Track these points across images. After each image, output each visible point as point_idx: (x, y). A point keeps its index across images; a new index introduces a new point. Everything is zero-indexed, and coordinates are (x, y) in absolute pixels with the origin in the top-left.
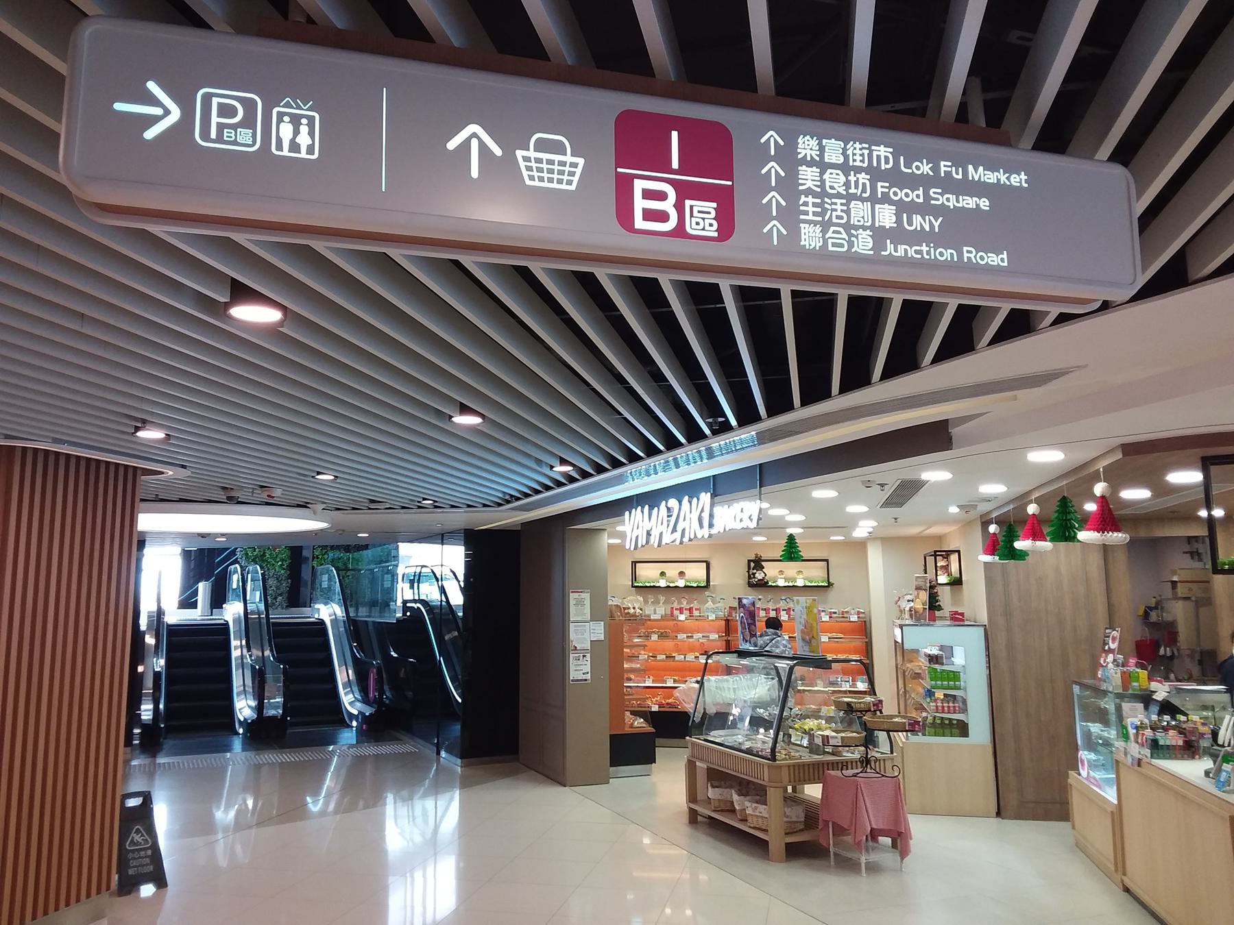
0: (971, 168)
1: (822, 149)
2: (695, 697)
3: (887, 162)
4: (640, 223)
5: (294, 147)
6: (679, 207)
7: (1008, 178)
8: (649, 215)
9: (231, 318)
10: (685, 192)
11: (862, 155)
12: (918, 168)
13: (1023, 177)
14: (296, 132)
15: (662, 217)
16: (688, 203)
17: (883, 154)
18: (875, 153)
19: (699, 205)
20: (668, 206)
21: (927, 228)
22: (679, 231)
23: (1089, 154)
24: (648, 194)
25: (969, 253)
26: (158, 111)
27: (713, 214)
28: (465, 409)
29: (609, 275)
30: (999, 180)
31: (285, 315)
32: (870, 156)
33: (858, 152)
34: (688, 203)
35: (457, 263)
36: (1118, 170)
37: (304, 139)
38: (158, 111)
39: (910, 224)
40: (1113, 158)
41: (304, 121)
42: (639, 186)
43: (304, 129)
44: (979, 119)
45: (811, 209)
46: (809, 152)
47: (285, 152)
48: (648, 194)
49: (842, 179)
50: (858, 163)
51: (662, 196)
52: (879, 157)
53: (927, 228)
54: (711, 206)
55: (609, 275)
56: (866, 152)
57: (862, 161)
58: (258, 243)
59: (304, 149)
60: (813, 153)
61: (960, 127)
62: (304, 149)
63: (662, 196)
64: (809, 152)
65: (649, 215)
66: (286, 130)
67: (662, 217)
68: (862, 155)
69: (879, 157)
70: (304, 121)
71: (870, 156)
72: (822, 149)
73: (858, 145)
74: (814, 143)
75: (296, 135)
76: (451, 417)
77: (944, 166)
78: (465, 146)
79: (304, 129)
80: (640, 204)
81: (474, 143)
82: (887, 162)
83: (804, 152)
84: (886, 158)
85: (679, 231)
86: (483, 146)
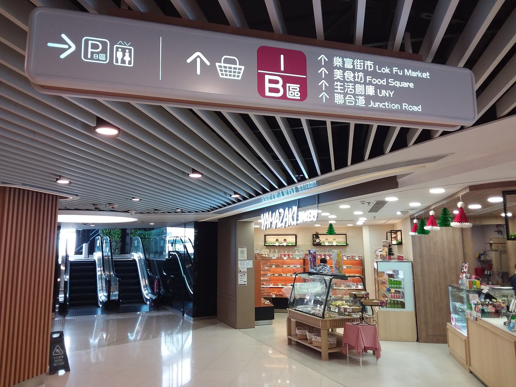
0: (406, 70)
1: (344, 62)
2: (291, 292)
3: (371, 68)
4: (267, 93)
5: (123, 61)
6: (284, 86)
7: (422, 75)
8: (271, 90)
9: (96, 133)
10: (286, 80)
11: (361, 65)
12: (384, 70)
13: (428, 74)
14: (124, 55)
15: (277, 91)
16: (288, 85)
17: (369, 65)
18: (366, 64)
19: (292, 86)
20: (279, 86)
21: (388, 96)
22: (284, 97)
23: (455, 64)
24: (271, 81)
25: (405, 106)
26: (66, 47)
27: (298, 90)
28: (194, 171)
29: (255, 115)
30: (418, 75)
31: (119, 132)
32: (364, 65)
33: (359, 63)
34: (288, 85)
35: (191, 110)
36: (468, 71)
37: (127, 58)
38: (66, 47)
39: (381, 94)
40: (466, 66)
41: (127, 51)
42: (267, 78)
43: (127, 54)
44: (409, 50)
45: (339, 87)
46: (338, 64)
47: (119, 64)
48: (271, 81)
49: (352, 75)
50: (359, 68)
51: (277, 82)
52: (367, 66)
53: (388, 96)
54: (297, 86)
55: (255, 115)
56: (362, 64)
57: (361, 67)
58: (108, 102)
59: (127, 62)
60: (340, 64)
61: (402, 53)
62: (127, 62)
63: (277, 82)
64: (338, 64)
65: (271, 90)
66: (120, 55)
67: (277, 91)
68: (361, 65)
69: (367, 66)
70: (127, 51)
71: (364, 65)
72: (344, 62)
73: (359, 61)
74: (340, 60)
75: (124, 56)
76: (189, 174)
77: (395, 70)
78: (195, 61)
79: (127, 54)
80: (268, 85)
81: (198, 60)
82: (371, 68)
83: (336, 64)
84: (371, 66)
85: (284, 97)
86: (202, 61)
